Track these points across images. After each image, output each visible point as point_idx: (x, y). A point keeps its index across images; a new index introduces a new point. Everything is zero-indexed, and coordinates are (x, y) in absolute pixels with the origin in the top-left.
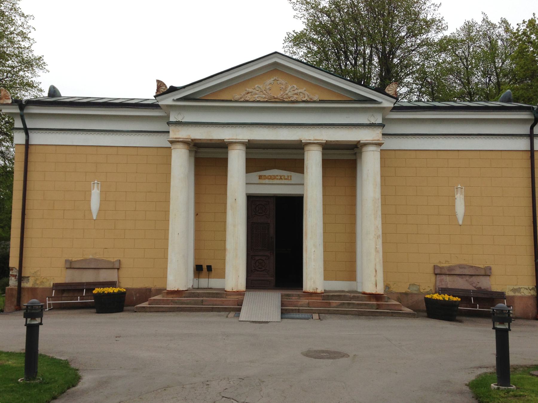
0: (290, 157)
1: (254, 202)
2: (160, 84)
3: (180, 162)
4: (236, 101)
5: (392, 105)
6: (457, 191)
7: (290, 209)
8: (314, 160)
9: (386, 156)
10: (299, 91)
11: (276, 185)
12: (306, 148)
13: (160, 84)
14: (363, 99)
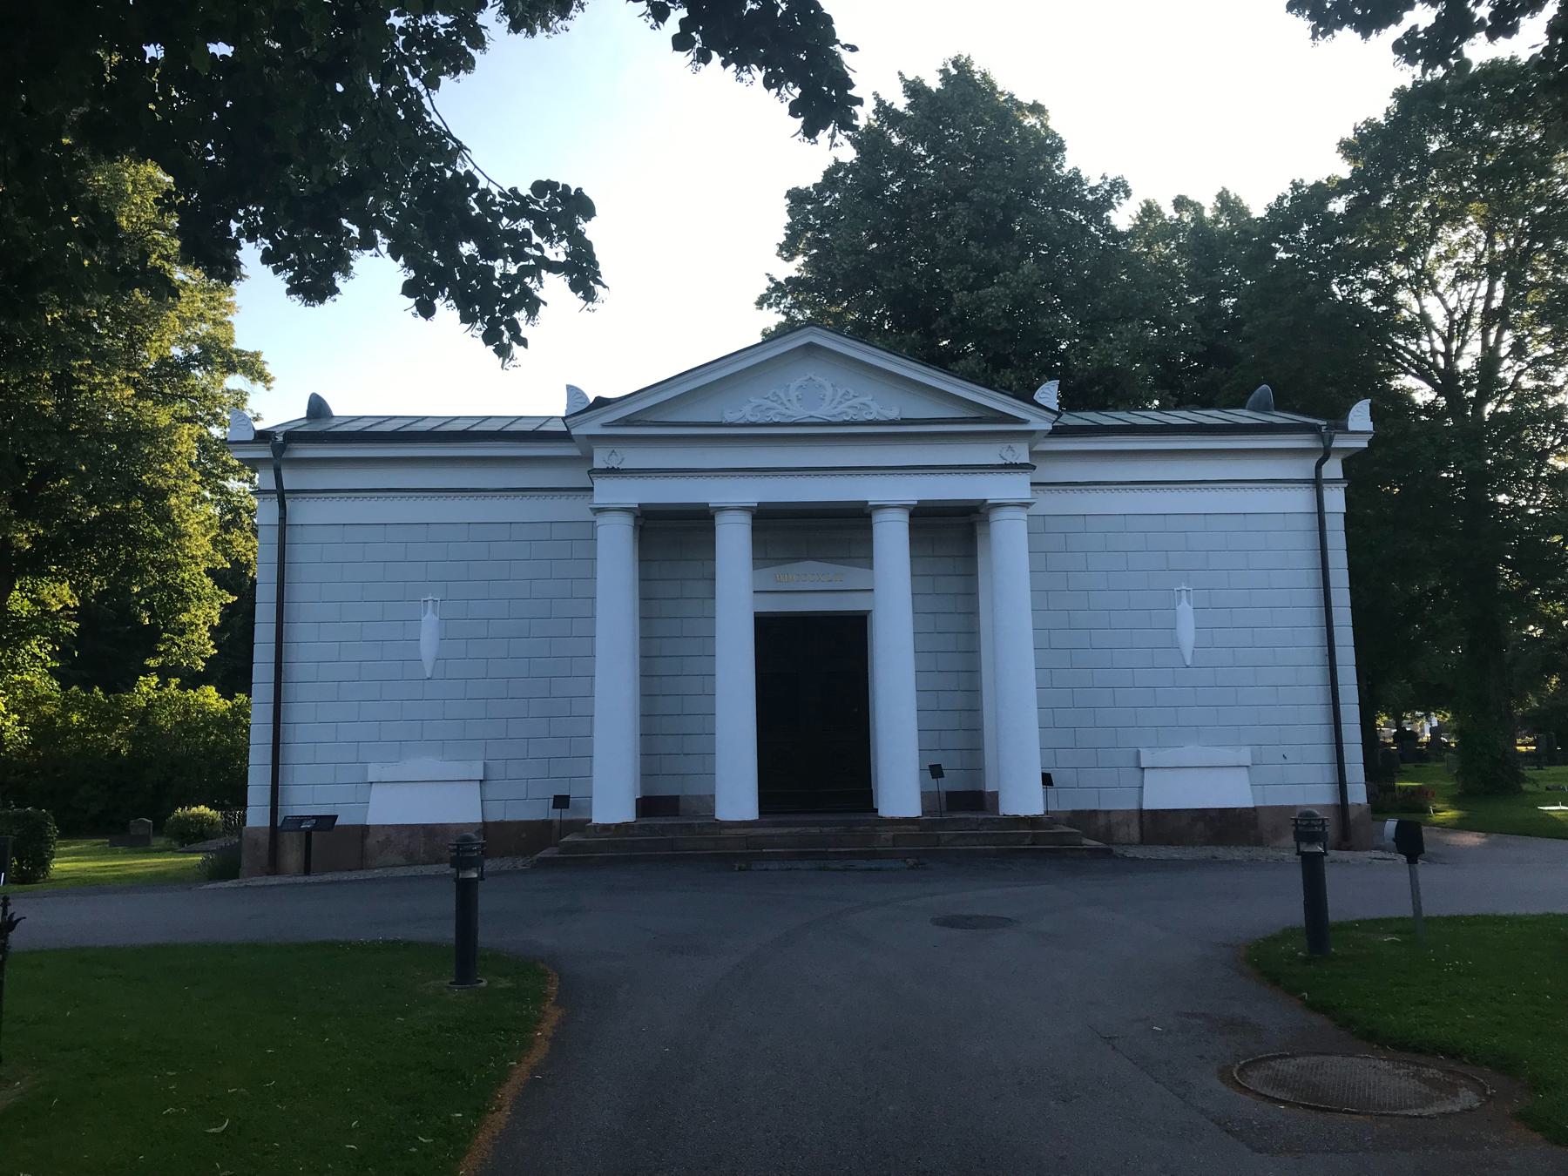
0: (841, 530)
1: (769, 629)
2: (573, 392)
3: (616, 547)
4: (731, 425)
5: (1049, 427)
6: (1180, 598)
7: (848, 636)
8: (892, 536)
9: (1039, 528)
10: (861, 400)
11: (812, 588)
12: (877, 518)
13: (573, 392)
14: (990, 414)
